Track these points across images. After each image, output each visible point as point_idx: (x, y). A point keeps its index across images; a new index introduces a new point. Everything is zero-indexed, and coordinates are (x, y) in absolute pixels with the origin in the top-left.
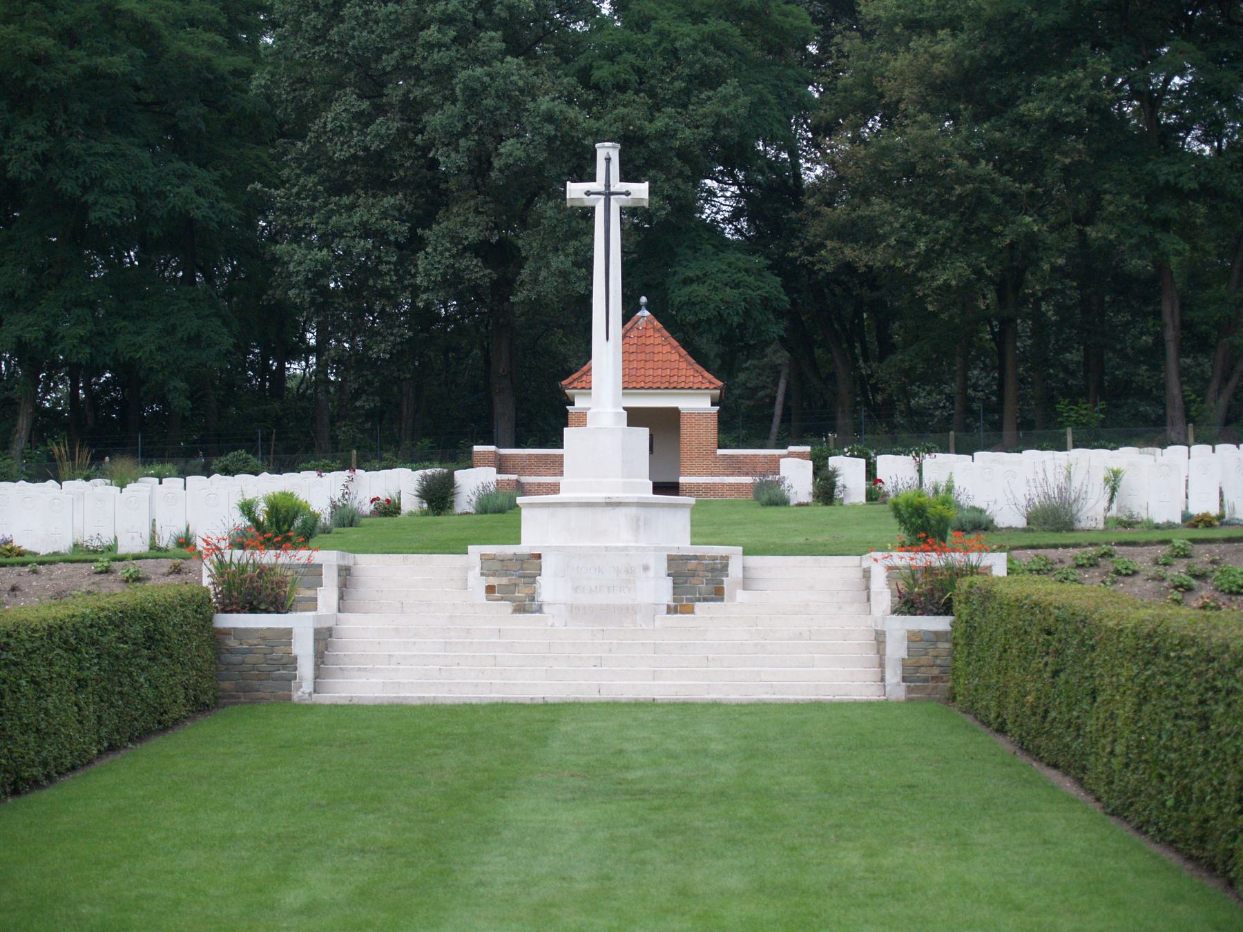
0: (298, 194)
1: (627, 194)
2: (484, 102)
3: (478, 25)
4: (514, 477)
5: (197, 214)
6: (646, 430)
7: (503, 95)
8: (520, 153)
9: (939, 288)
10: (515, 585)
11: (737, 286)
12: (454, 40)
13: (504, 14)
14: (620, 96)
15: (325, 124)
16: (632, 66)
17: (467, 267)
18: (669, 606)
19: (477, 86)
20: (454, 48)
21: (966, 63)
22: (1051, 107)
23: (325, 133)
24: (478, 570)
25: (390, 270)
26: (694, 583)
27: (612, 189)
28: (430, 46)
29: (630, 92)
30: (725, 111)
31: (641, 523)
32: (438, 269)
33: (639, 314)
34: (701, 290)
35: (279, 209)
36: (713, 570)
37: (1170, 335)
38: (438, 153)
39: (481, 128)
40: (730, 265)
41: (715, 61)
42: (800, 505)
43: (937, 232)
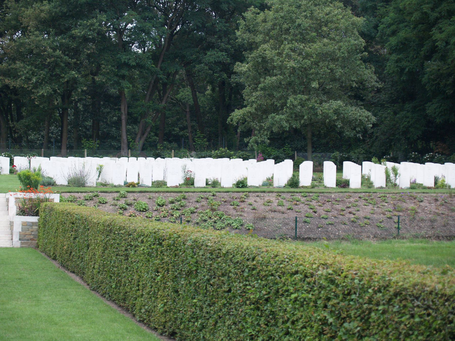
9: (40, 96)
43: (40, 75)
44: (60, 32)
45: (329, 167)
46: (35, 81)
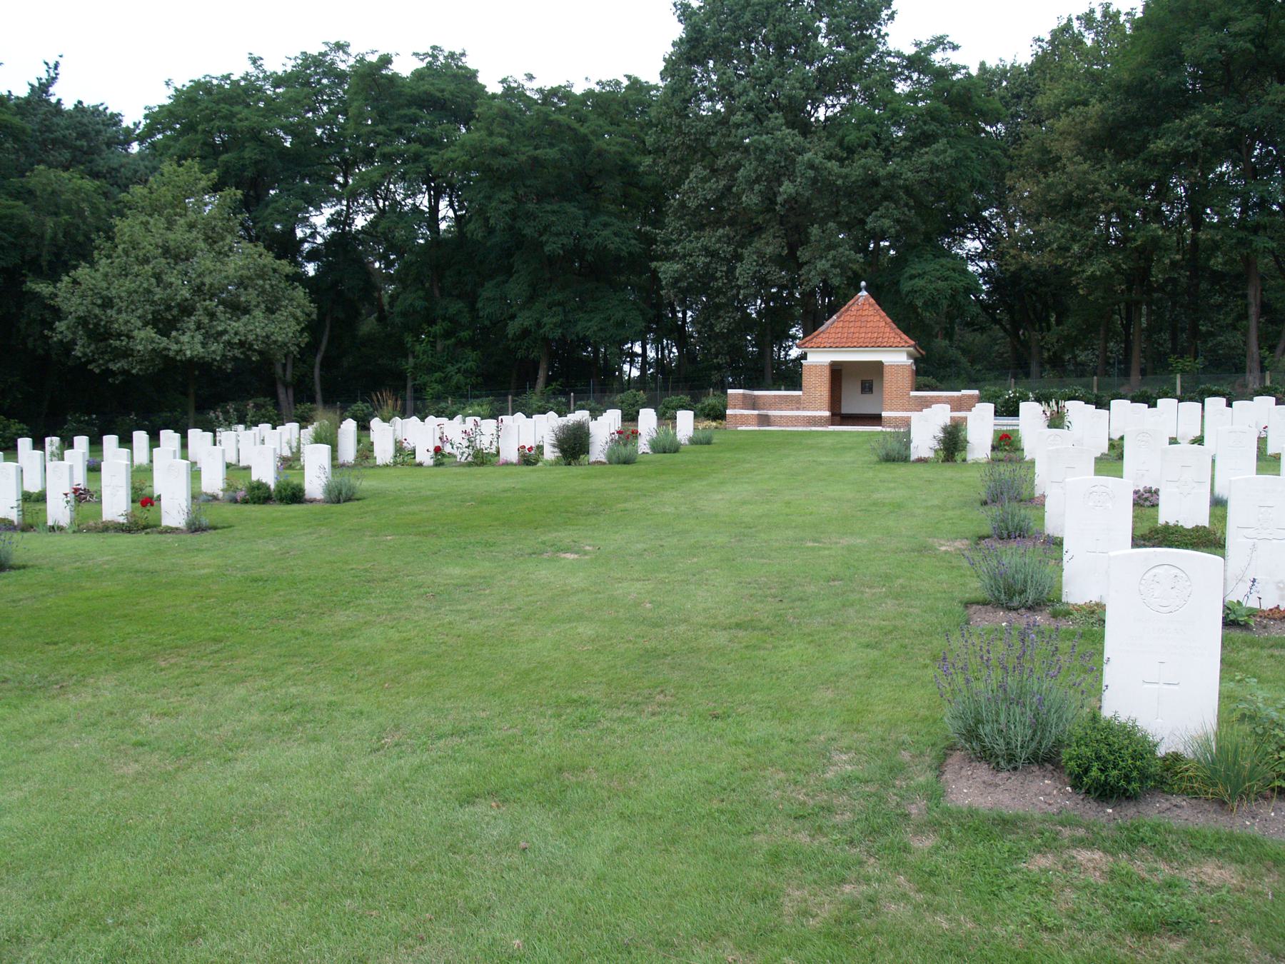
5: (611, 246)
7: (781, 152)
9: (1088, 278)
11: (946, 279)
12: (753, 121)
34: (919, 283)
37: (1253, 310)
41: (932, 127)
42: (920, 460)
44: (1122, 154)
45: (647, 419)
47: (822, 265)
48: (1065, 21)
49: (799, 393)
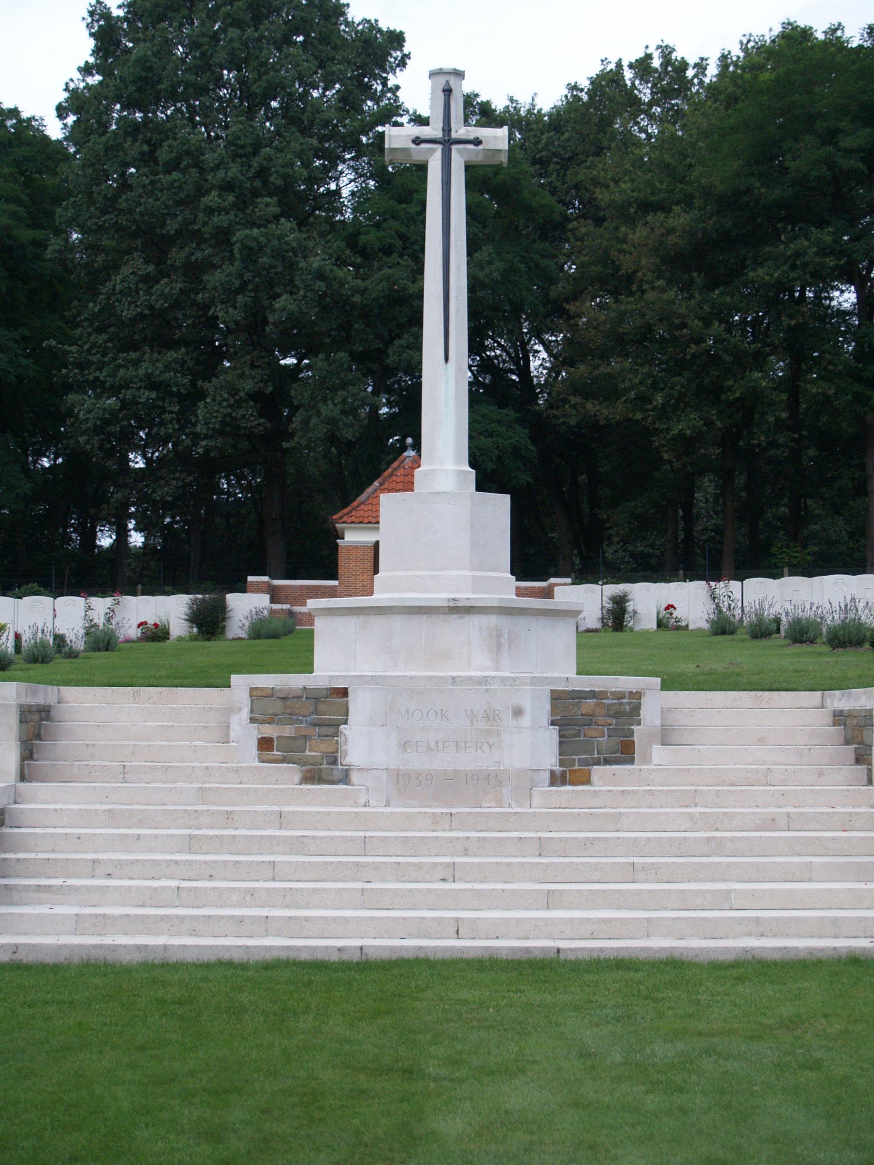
0: (89, 351)
1: (477, 142)
2: (261, 260)
3: (255, 194)
4: (286, 607)
6: (507, 498)
7: (277, 254)
8: (293, 307)
10: (306, 738)
12: (234, 205)
13: (279, 182)
14: (385, 259)
15: (114, 286)
16: (397, 232)
17: (243, 416)
18: (553, 773)
19: (254, 245)
20: (232, 213)
21: (700, 234)
22: (779, 272)
23: (114, 294)
24: (245, 713)
25: (172, 419)
26: (592, 735)
27: (454, 135)
28: (211, 211)
29: (395, 255)
30: (481, 274)
31: (504, 640)
32: (216, 417)
33: (405, 454)
35: (72, 364)
36: (618, 714)
38: (219, 310)
39: (258, 286)
40: (483, 416)
43: (672, 388)
46: (661, 401)
47: (328, 410)
48: (612, 66)
49: (335, 583)
